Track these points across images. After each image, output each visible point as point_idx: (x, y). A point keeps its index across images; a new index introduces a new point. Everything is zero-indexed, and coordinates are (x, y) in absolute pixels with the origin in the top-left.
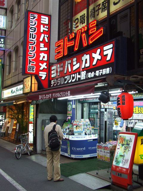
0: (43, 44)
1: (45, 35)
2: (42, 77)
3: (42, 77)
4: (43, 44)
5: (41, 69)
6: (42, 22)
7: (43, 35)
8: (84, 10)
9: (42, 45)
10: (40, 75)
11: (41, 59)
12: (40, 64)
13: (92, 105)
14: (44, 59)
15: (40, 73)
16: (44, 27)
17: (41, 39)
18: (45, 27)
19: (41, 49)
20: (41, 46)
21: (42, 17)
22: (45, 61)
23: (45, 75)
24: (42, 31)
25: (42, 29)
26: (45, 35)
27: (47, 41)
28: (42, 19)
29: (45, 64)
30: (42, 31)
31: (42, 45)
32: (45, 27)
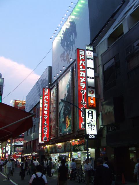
0: (82, 67)
1: (83, 61)
2: (82, 86)
3: (82, 86)
4: (82, 67)
5: (45, 110)
6: (80, 54)
7: (45, 96)
8: (126, 33)
9: (45, 100)
10: (81, 85)
11: (45, 106)
12: (45, 108)
13: (22, 145)
14: (83, 76)
15: (81, 84)
16: (82, 56)
17: (45, 98)
18: (83, 56)
19: (45, 102)
20: (80, 68)
21: (80, 50)
22: (84, 77)
23: (85, 86)
24: (80, 59)
25: (45, 94)
26: (83, 61)
27: (84, 65)
28: (80, 52)
29: (84, 78)
30: (80, 59)
31: (81, 67)
32: (83, 56)
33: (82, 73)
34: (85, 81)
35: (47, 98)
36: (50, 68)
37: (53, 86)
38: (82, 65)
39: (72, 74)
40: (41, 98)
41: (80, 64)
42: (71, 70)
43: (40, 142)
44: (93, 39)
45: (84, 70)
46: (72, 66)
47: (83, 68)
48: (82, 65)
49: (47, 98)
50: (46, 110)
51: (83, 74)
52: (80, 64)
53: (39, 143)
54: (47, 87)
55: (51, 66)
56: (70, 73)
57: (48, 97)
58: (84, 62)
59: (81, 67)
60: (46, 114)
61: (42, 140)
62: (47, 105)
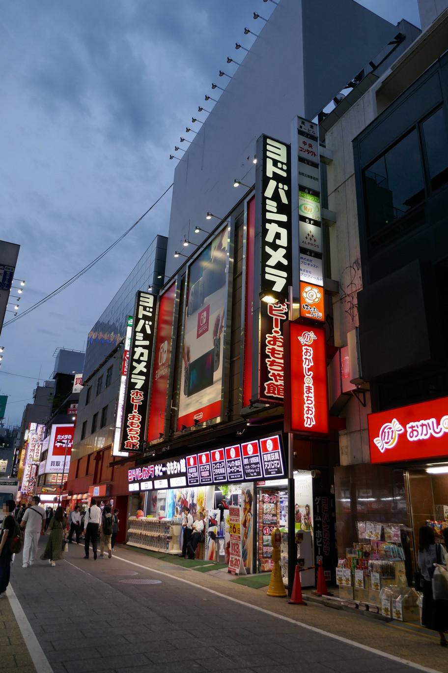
0: (142, 335)
1: (280, 185)
2: (274, 283)
3: (274, 283)
27: (284, 200)
31: (271, 205)
33: (273, 229)
34: (285, 262)
35: (149, 331)
36: (163, 243)
37: (166, 288)
38: (276, 197)
39: (233, 245)
40: (131, 322)
41: (269, 193)
42: (229, 229)
43: (116, 452)
44: (242, 203)
45: (283, 218)
46: (235, 213)
47: (280, 211)
48: (276, 197)
49: (149, 331)
50: (141, 373)
51: (278, 236)
52: (269, 193)
53: (115, 457)
54: (150, 289)
55: (167, 236)
56: (396, 44)
57: (152, 327)
58: (286, 188)
59: (271, 205)
60: (138, 386)
61: (122, 449)
62: (146, 352)
